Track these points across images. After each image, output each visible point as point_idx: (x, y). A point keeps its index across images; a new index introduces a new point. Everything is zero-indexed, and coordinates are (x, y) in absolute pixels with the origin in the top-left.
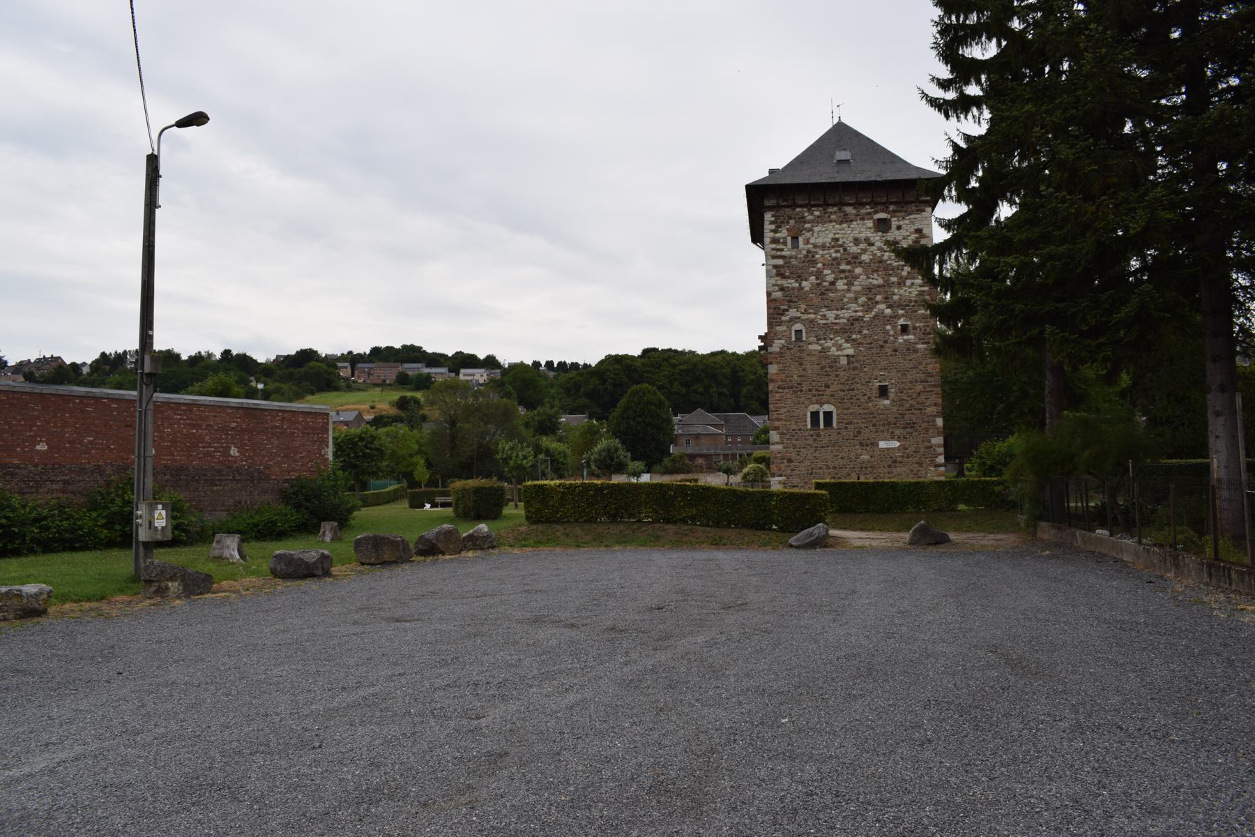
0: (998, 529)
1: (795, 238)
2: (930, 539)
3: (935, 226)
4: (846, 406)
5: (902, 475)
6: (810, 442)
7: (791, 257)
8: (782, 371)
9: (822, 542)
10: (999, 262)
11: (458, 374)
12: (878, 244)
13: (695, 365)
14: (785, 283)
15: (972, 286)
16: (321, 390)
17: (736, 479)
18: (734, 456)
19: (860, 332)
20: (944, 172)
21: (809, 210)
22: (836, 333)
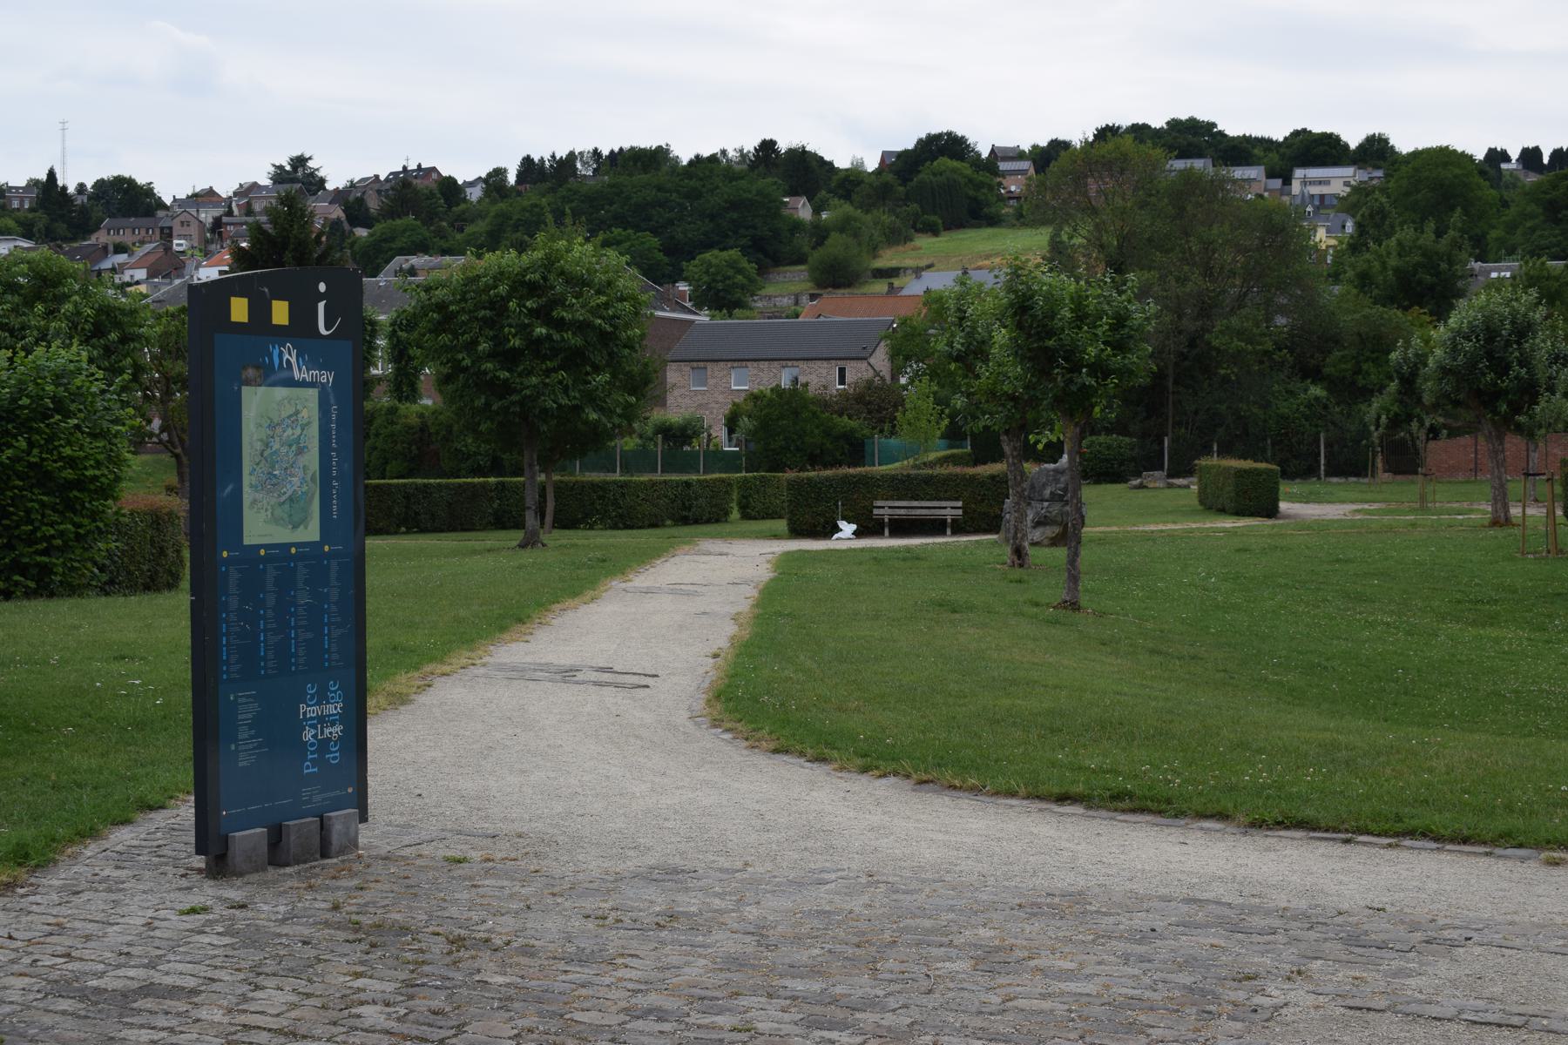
11: (1287, 181)
16: (955, 223)
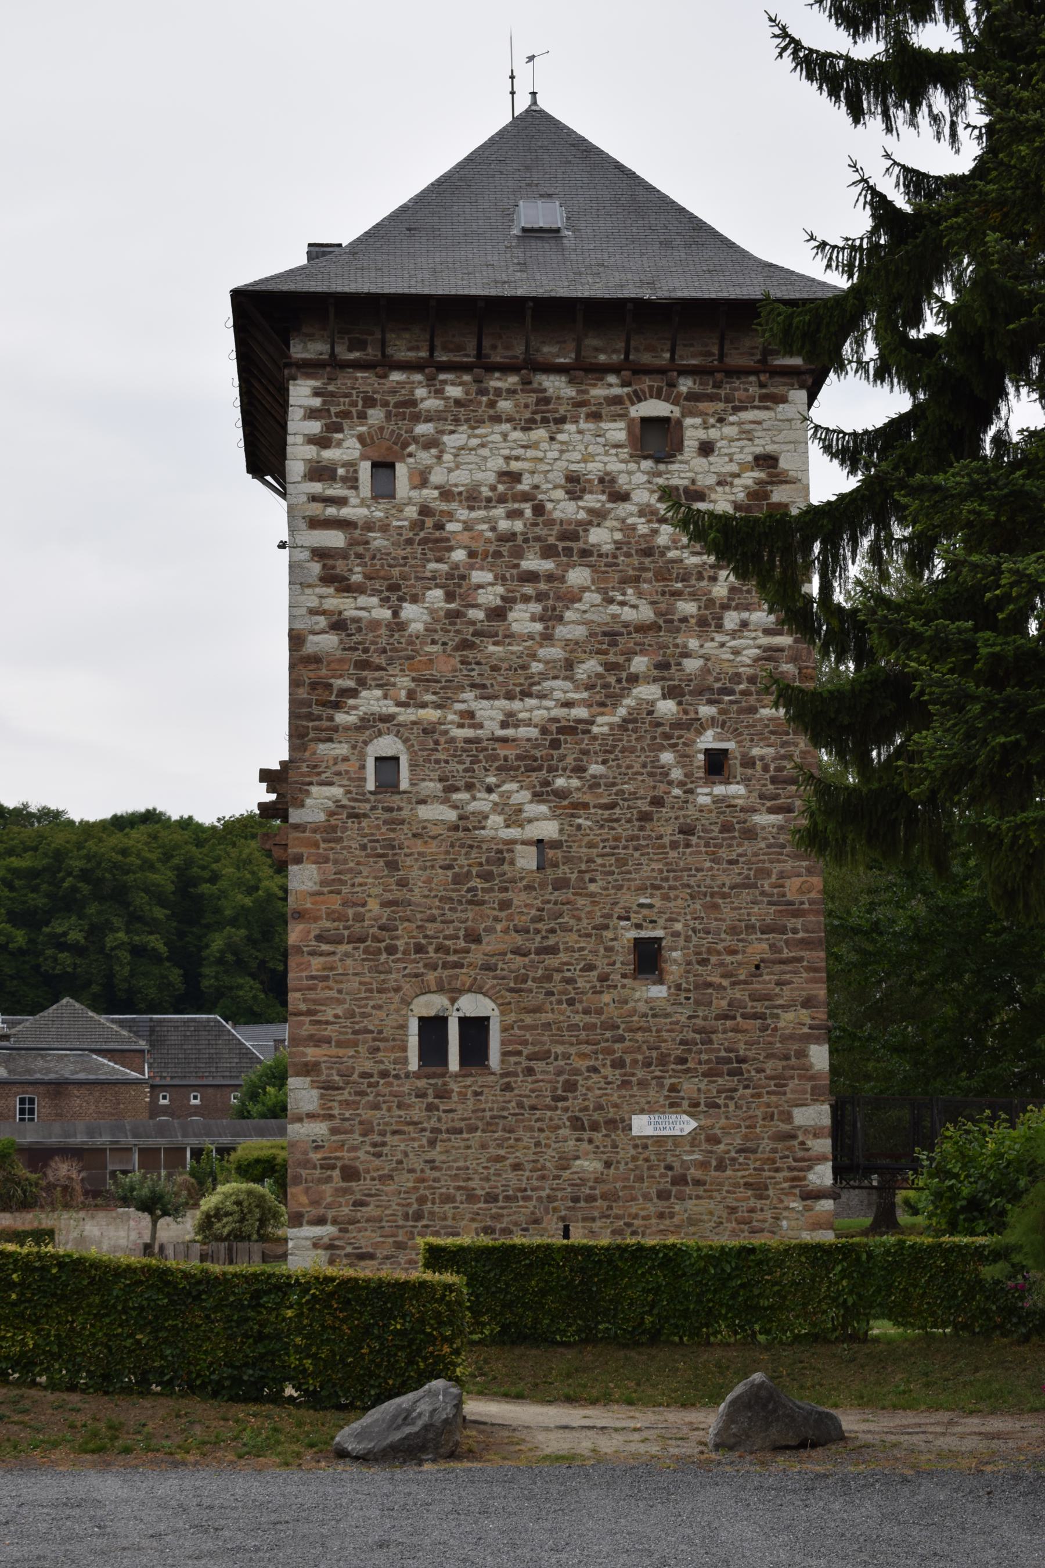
0: (993, 1402)
1: (383, 467)
2: (783, 1431)
3: (815, 449)
4: (529, 1001)
5: (703, 1224)
6: (417, 1113)
7: (369, 526)
8: (331, 885)
9: (441, 1443)
10: (997, 571)
12: (642, 496)
13: (59, 856)
14: (349, 606)
15: (915, 639)
17: (178, 1231)
18: (176, 1153)
19: (579, 770)
20: (841, 281)
21: (431, 380)
22: (505, 769)
